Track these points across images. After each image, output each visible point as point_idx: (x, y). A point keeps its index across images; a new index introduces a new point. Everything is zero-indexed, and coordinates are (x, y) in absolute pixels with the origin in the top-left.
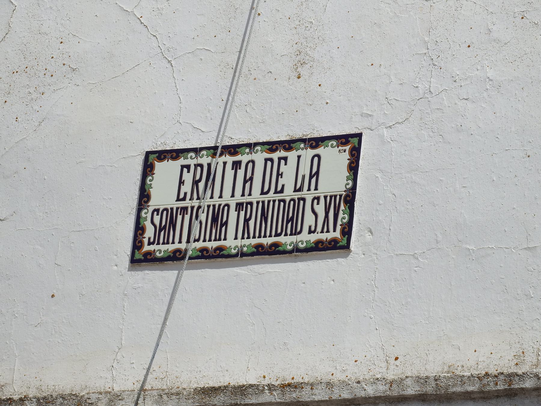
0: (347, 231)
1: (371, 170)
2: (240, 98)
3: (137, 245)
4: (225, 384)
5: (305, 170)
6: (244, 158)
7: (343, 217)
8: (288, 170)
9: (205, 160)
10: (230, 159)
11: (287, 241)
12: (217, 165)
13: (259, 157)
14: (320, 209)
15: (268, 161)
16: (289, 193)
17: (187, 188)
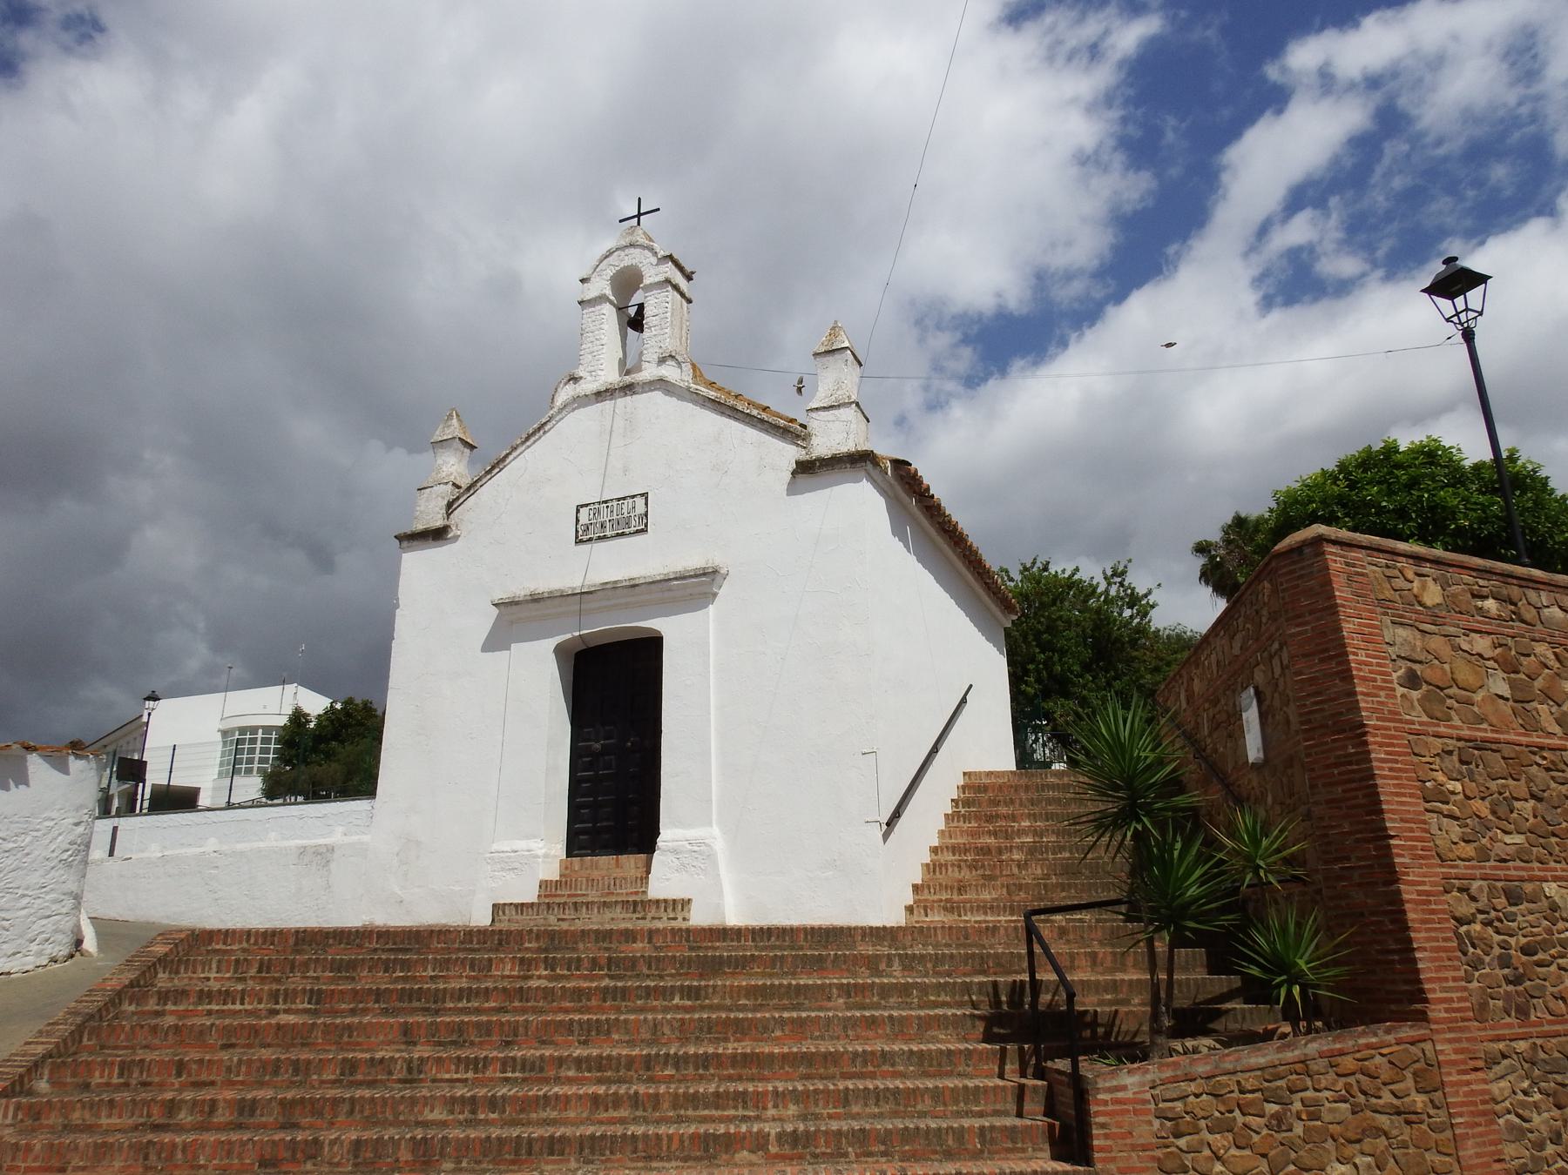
0: (646, 526)
1: (1485, 1044)
2: (606, 484)
3: (577, 537)
4: (333, 866)
5: (630, 506)
6: (609, 504)
7: (645, 521)
8: (625, 507)
9: (597, 506)
10: (605, 505)
11: (627, 531)
12: (1560, 587)
13: (615, 503)
14: (637, 519)
15: (1222, 604)
16: (626, 515)
17: (592, 516)
